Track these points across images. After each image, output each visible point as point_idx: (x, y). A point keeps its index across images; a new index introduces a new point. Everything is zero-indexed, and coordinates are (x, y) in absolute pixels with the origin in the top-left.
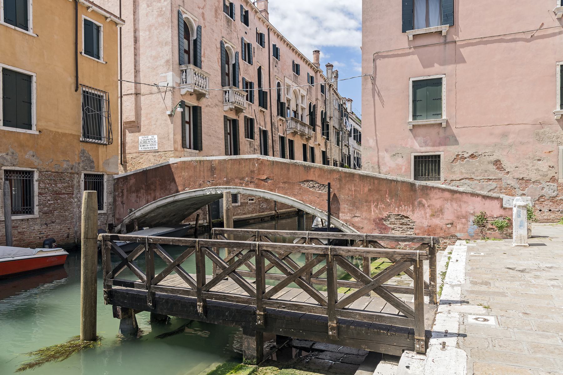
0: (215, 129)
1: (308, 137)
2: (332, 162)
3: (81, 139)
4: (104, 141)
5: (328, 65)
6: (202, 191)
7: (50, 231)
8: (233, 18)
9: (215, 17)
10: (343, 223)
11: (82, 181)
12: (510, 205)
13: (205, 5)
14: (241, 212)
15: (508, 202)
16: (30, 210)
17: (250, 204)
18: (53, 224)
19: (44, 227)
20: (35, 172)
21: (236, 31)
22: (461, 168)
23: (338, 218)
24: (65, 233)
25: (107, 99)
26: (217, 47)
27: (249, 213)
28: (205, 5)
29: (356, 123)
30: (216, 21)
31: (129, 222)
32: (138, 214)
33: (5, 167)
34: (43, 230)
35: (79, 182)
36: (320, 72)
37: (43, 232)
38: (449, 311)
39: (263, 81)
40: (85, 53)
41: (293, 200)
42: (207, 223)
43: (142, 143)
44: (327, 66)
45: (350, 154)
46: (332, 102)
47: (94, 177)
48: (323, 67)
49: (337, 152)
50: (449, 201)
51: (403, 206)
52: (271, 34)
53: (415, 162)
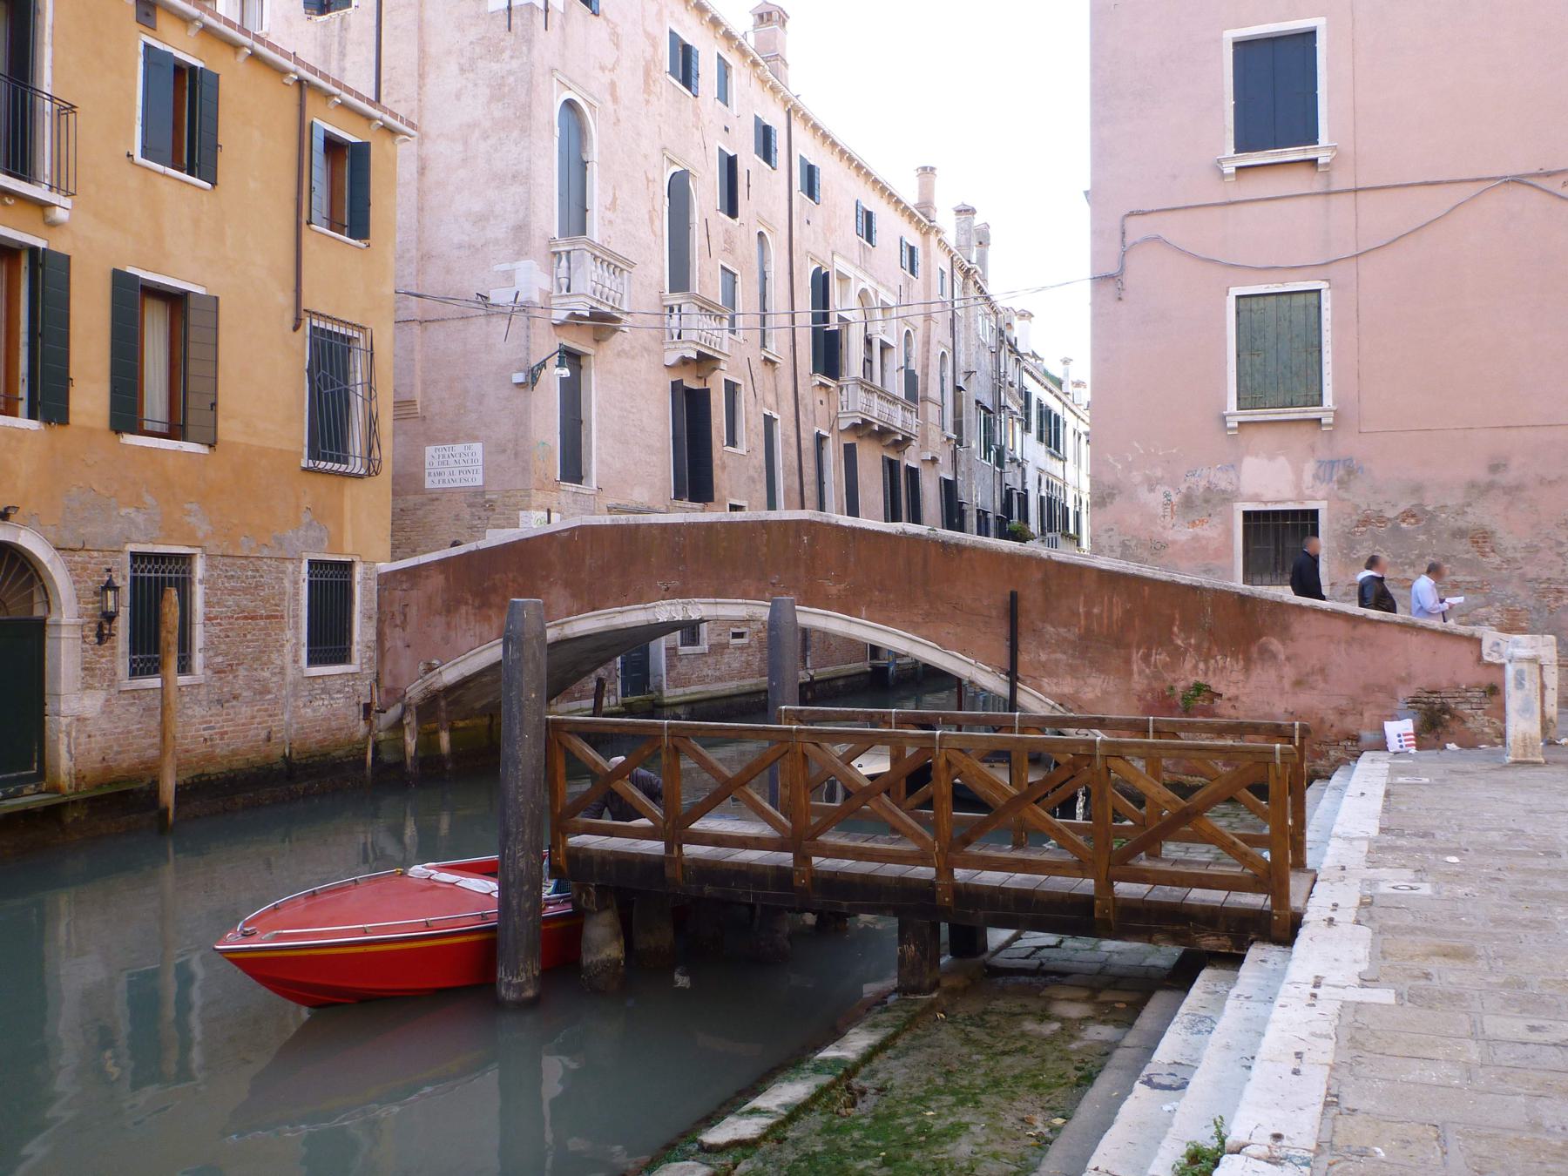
0: (641, 421)
1: (903, 436)
2: (972, 521)
3: (304, 464)
4: (356, 465)
5: (961, 208)
6: (643, 611)
7: (227, 721)
8: (690, 91)
9: (644, 92)
10: (1052, 703)
11: (304, 580)
12: (1501, 656)
13: (618, 60)
14: (710, 672)
15: (1495, 649)
16: (156, 664)
17: (735, 649)
18: (234, 703)
19: (216, 709)
20: (198, 556)
21: (700, 125)
22: (1377, 547)
23: (1039, 689)
24: (263, 729)
25: (369, 349)
26: (647, 178)
27: (732, 678)
28: (618, 60)
29: (1046, 388)
30: (647, 102)
31: (423, 699)
32: (450, 675)
33: (133, 545)
34: (213, 719)
35: (296, 583)
36: (938, 232)
37: (212, 724)
38: (1333, 910)
39: (773, 270)
40: (145, 155)
41: (911, 639)
42: (617, 704)
43: (436, 465)
44: (959, 212)
45: (1028, 487)
46: (972, 325)
47: (331, 569)
48: (946, 220)
49: (989, 481)
50: (1343, 646)
51: (1219, 657)
52: (797, 127)
53: (1246, 529)
